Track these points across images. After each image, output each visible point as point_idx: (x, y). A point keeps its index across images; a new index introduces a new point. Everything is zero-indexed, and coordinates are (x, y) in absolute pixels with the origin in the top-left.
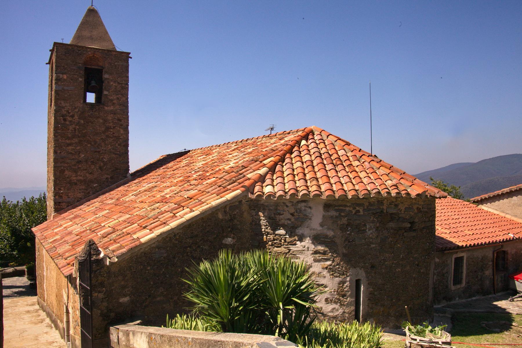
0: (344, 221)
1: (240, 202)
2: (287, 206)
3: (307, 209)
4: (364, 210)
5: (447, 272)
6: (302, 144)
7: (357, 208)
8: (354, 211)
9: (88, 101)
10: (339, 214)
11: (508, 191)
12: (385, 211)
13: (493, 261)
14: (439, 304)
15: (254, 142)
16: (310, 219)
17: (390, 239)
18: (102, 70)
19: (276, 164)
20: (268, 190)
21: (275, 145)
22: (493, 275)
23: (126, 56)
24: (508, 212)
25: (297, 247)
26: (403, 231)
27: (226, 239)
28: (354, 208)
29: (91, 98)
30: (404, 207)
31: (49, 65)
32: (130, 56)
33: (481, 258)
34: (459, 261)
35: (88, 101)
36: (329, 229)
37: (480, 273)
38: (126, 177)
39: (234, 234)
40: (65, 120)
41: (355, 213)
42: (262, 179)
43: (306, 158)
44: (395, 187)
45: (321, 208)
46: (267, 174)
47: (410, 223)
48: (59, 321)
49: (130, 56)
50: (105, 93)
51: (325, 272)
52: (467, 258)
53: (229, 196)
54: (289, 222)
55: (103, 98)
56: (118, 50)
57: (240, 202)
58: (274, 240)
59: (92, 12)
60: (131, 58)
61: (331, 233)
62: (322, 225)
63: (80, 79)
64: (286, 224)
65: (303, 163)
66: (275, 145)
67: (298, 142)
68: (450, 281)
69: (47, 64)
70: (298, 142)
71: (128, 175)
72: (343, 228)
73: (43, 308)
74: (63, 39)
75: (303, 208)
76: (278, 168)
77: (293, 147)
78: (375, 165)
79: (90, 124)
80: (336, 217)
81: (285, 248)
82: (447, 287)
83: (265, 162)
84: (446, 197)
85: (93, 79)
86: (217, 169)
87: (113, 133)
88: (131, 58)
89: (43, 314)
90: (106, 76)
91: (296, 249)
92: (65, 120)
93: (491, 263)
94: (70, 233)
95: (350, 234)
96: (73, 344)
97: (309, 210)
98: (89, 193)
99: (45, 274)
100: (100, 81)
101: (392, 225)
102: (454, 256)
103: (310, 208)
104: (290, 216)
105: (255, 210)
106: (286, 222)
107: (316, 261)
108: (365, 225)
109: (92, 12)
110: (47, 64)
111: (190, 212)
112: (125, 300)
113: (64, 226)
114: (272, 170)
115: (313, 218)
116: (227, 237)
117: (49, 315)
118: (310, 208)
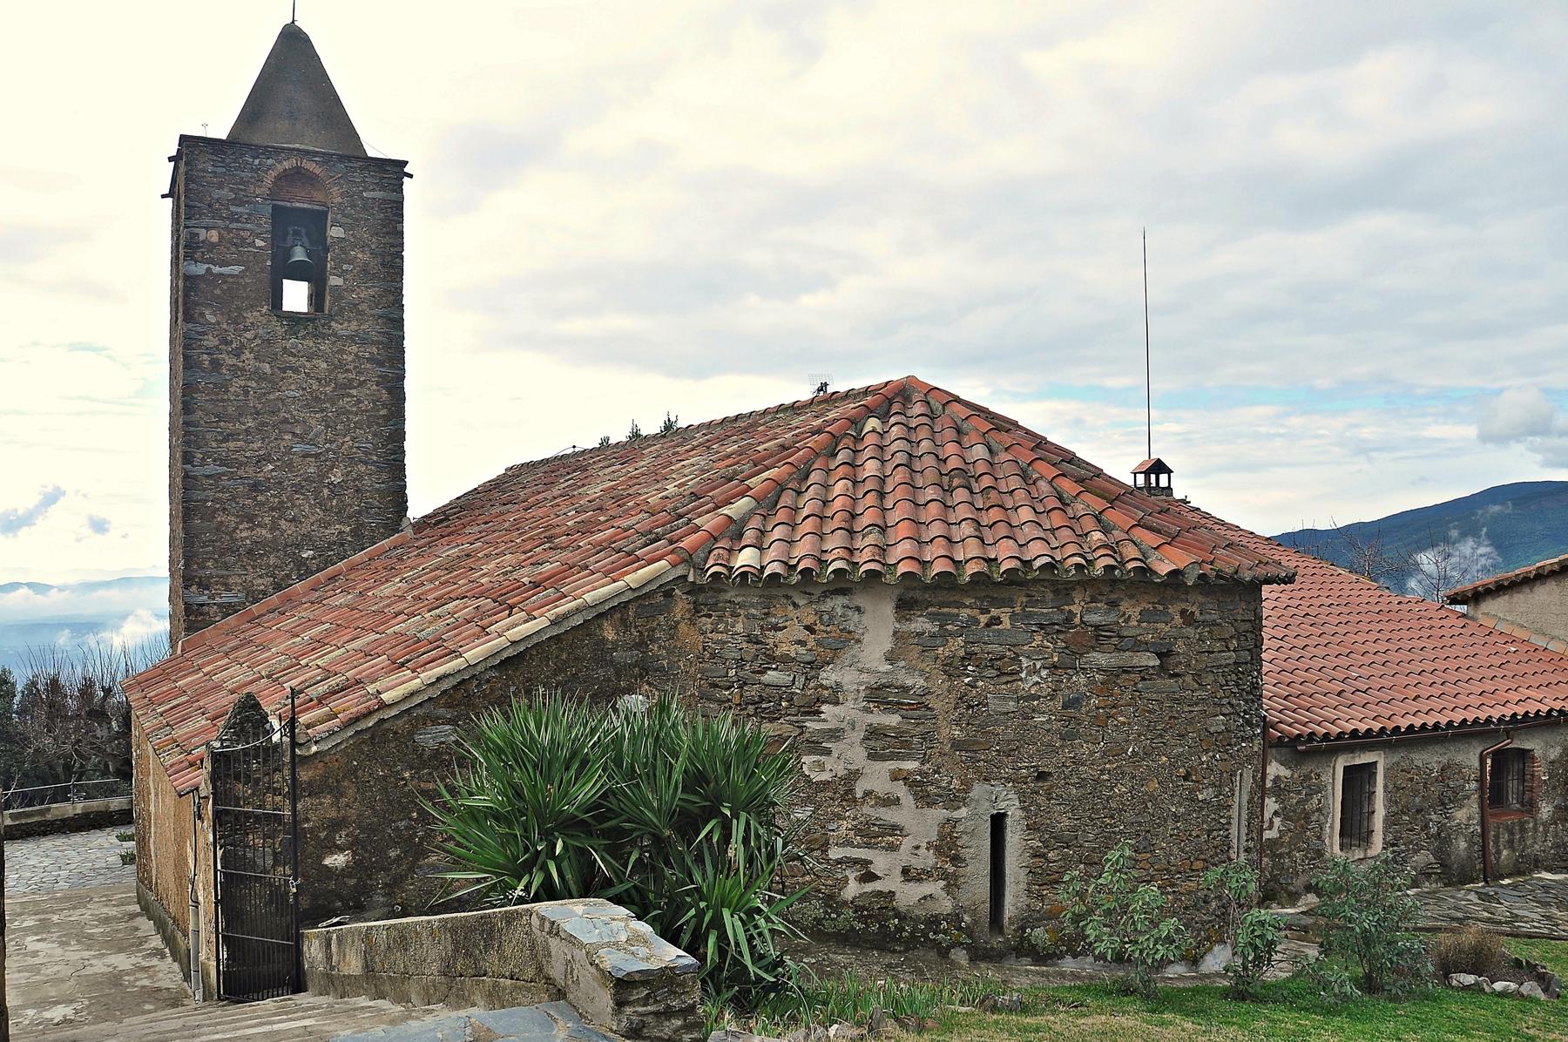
0: (957, 645)
3: (850, 613)
4: (1013, 617)
5: (1319, 810)
6: (867, 428)
7: (994, 612)
8: (983, 619)
9: (286, 308)
10: (941, 626)
11: (1556, 567)
12: (1077, 620)
13: (1481, 780)
14: (1293, 905)
15: (751, 425)
16: (858, 641)
17: (1094, 701)
18: (326, 214)
19: (780, 487)
20: (746, 558)
22: (1483, 823)
24: (1555, 633)
25: (824, 720)
26: (1137, 677)
27: (626, 697)
28: (985, 611)
29: (296, 296)
30: (1138, 609)
31: (170, 200)
32: (406, 170)
33: (1437, 768)
35: (286, 308)
36: (910, 669)
37: (1434, 817)
39: (649, 684)
41: (988, 625)
42: (734, 532)
43: (871, 468)
45: (888, 609)
46: (751, 513)
47: (1160, 655)
48: (179, 935)
49: (406, 170)
50: (334, 281)
51: (901, 790)
52: (1387, 770)
53: (636, 577)
54: (802, 650)
56: (371, 153)
58: (762, 700)
59: (293, 56)
60: (411, 176)
61: (915, 681)
62: (891, 658)
64: (793, 655)
65: (855, 483)
67: (856, 422)
68: (1331, 837)
69: (163, 196)
70: (856, 422)
71: (405, 523)
72: (952, 669)
73: (147, 910)
75: (839, 611)
76: (787, 499)
77: (836, 438)
78: (1068, 486)
79: (290, 373)
80: (933, 636)
81: (791, 723)
82: (1319, 853)
87: (359, 401)
88: (411, 176)
89: (146, 925)
91: (818, 726)
93: (1474, 785)
94: (218, 687)
95: (972, 685)
96: (12, 524)
97: (856, 617)
98: (288, 576)
99: (152, 809)
100: (319, 245)
101: (1101, 659)
102: (1341, 763)
103: (858, 609)
104: (803, 634)
105: (710, 616)
106: (793, 650)
107: (873, 756)
108: (1016, 659)
109: (293, 56)
110: (163, 196)
111: (526, 621)
113: (206, 670)
114: (768, 504)
115: (866, 638)
116: (630, 690)
117: (161, 927)
118: (858, 609)
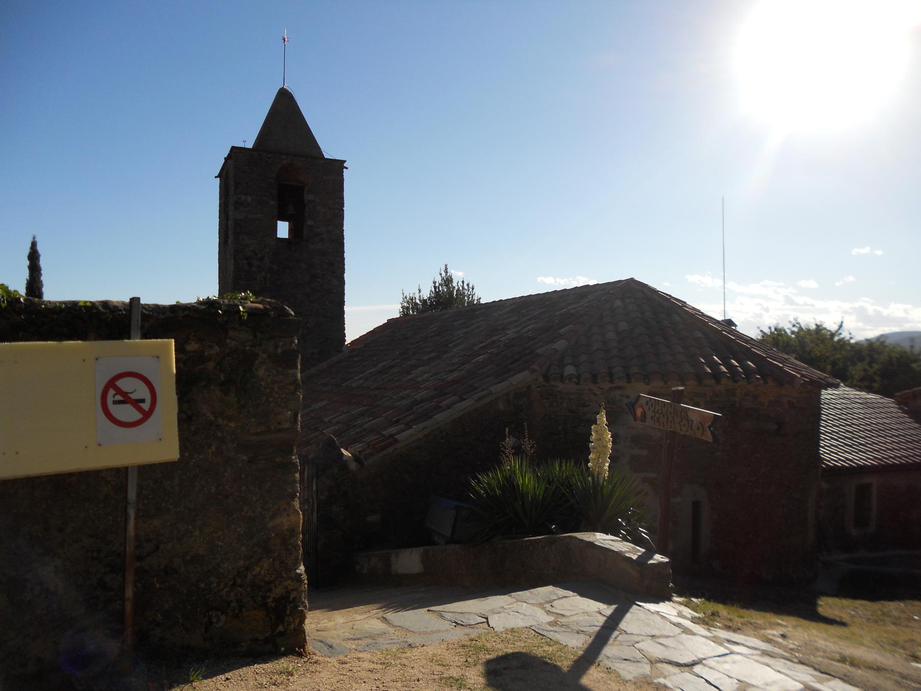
1: (529, 387)
2: (595, 394)
21: (574, 306)
23: (338, 166)
29: (283, 230)
32: (345, 165)
34: (863, 491)
38: (341, 351)
40: (250, 265)
44: (485, 620)
49: (345, 165)
50: (310, 222)
55: (305, 232)
56: (326, 156)
57: (529, 387)
63: (272, 203)
66: (574, 306)
71: (344, 349)
74: (244, 141)
83: (562, 331)
84: (906, 642)
85: (290, 203)
86: (489, 341)
90: (308, 197)
92: (250, 265)
112: (373, 518)
